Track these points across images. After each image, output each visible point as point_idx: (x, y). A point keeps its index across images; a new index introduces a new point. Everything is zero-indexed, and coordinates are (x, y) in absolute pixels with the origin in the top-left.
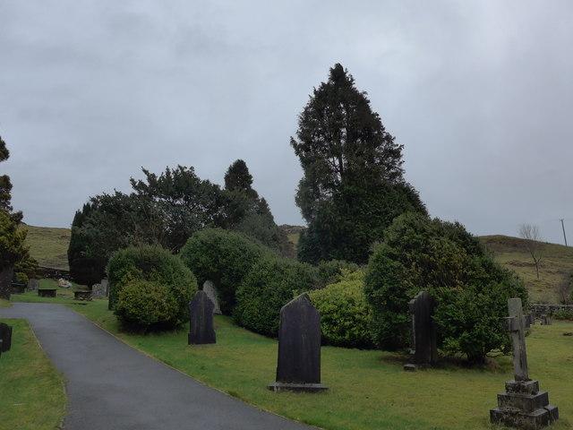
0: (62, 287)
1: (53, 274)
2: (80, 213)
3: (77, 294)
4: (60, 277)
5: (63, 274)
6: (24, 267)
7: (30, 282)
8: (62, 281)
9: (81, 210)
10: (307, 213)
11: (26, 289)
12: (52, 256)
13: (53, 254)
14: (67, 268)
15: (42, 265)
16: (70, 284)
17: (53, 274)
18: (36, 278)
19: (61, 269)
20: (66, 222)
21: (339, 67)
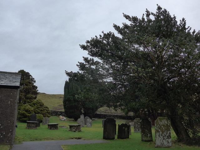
0: (61, 120)
1: (57, 114)
2: (67, 82)
3: (71, 127)
4: (60, 115)
5: (61, 114)
6: (41, 111)
7: (44, 119)
8: (61, 117)
9: (68, 80)
10: (65, 108)
11: (41, 124)
12: (56, 105)
13: (59, 105)
14: (63, 110)
15: (51, 109)
16: (65, 118)
17: (57, 114)
18: (48, 117)
19: (61, 111)
20: (61, 92)
21: (183, 18)
